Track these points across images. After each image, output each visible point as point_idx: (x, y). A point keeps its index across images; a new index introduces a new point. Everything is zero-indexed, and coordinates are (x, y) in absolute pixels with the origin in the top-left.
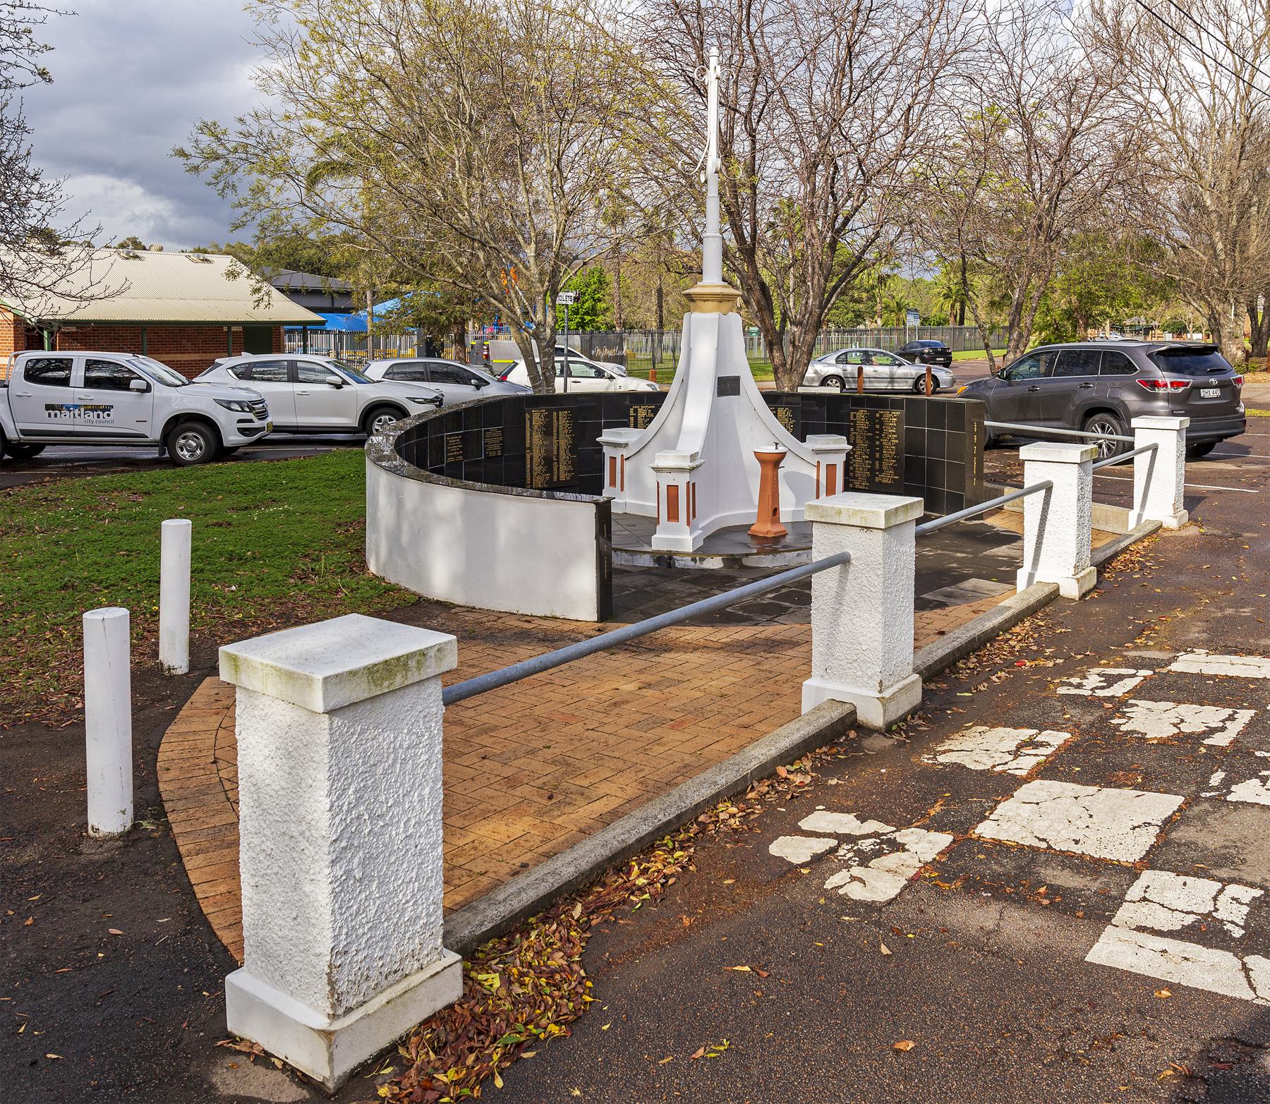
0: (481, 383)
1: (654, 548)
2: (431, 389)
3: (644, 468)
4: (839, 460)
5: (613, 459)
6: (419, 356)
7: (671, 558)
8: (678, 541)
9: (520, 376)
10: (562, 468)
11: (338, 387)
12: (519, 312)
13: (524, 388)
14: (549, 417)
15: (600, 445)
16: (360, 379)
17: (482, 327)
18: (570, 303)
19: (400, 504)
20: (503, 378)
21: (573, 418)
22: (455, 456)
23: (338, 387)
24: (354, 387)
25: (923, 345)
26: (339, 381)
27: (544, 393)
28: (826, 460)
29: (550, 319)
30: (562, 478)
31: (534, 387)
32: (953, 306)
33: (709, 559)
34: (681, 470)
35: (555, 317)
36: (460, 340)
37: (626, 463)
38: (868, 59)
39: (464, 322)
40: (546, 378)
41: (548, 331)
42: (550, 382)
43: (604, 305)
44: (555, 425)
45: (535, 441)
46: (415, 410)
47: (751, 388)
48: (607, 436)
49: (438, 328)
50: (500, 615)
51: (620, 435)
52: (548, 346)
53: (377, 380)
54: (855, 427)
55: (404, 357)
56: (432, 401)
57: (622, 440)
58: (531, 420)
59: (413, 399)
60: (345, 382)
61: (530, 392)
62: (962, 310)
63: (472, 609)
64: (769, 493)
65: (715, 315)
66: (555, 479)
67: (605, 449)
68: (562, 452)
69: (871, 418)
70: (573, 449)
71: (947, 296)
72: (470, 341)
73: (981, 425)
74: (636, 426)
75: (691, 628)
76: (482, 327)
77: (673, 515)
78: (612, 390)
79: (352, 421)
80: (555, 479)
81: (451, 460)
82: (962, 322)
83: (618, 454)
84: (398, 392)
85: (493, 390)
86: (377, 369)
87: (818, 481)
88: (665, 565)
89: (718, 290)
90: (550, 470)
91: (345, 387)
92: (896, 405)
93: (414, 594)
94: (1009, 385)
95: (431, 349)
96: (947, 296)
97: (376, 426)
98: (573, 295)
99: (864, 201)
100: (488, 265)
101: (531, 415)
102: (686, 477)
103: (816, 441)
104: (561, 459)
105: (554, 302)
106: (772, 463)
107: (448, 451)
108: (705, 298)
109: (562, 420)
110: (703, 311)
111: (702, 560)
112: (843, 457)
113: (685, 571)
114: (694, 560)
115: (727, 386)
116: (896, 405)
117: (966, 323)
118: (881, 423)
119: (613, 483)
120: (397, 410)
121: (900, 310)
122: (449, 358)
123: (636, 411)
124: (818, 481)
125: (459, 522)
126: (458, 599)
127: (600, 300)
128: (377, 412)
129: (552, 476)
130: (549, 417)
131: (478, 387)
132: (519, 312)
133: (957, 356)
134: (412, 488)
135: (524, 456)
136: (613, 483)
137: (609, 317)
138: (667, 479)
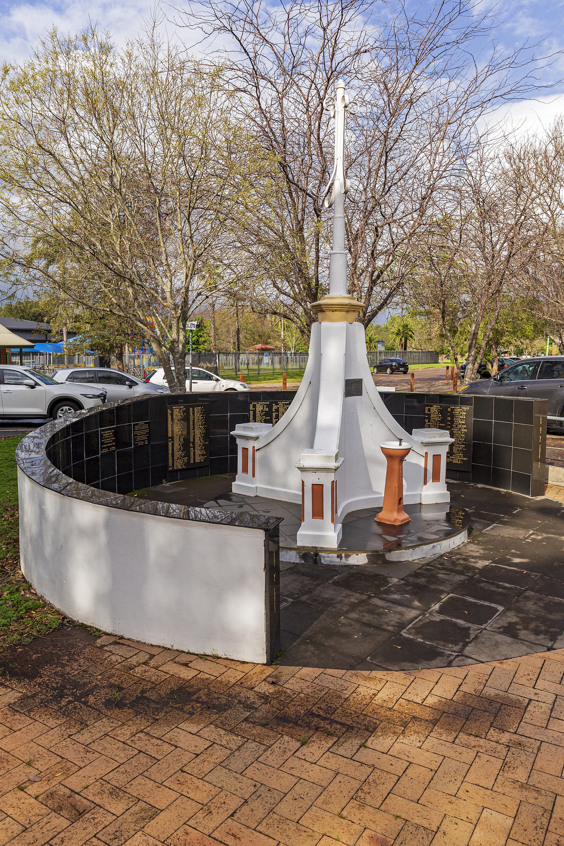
0: (133, 384)
1: (299, 544)
2: (99, 388)
3: (279, 463)
4: (443, 451)
5: (245, 450)
6: (95, 366)
7: (316, 555)
8: (321, 537)
9: (159, 378)
10: (198, 452)
11: (32, 387)
12: (159, 333)
13: (162, 387)
14: (187, 412)
15: (233, 439)
16: (50, 382)
17: (134, 351)
18: (194, 329)
19: (42, 513)
20: (147, 381)
21: (206, 413)
22: (108, 447)
23: (32, 387)
24: (43, 387)
25: (392, 361)
26: (31, 382)
27: (178, 392)
28: (432, 451)
29: (181, 338)
30: (197, 460)
31: (170, 387)
32: (401, 340)
33: (354, 556)
34: (327, 470)
35: (185, 336)
36: (120, 357)
37: (257, 454)
38: (399, 161)
39: (122, 347)
40: (179, 381)
41: (181, 346)
42: (182, 384)
43: (204, 339)
44: (191, 418)
45: (175, 428)
46: (88, 404)
47: (372, 390)
48: (239, 430)
49: (106, 353)
50: (154, 652)
51: (251, 429)
52: (180, 357)
53: (62, 383)
54: (429, 419)
55: (88, 367)
56: (98, 396)
57: (253, 434)
58: (172, 415)
59: (85, 395)
60: (37, 384)
61: (168, 392)
62: (406, 342)
63: (120, 641)
64: (396, 484)
65: (343, 324)
66: (192, 461)
67: (238, 441)
68: (197, 440)
69: (443, 412)
70: (206, 436)
71: (397, 334)
72: (126, 359)
73: (544, 419)
74: (255, 420)
75: (378, 674)
76: (134, 351)
77: (318, 513)
78: (217, 390)
79: (42, 410)
80: (192, 461)
81: (106, 450)
82: (405, 349)
83: (250, 445)
84: (75, 390)
85: (140, 390)
86: (62, 375)
87: (426, 469)
88: (311, 562)
89: (347, 301)
90: (188, 455)
91: (38, 388)
92: (464, 401)
93: (58, 612)
94: (501, 385)
95: (103, 362)
96: (397, 334)
97: (60, 413)
98: (196, 323)
99: (392, 261)
100: (136, 299)
101: (172, 410)
102: (331, 477)
103: (422, 435)
104: (197, 446)
105: (184, 325)
106: (395, 459)
107: (102, 443)
108: (334, 308)
109: (197, 414)
110: (331, 320)
111: (347, 556)
112: (446, 449)
113: (332, 569)
114: (340, 557)
115: (353, 388)
116: (464, 401)
117: (408, 350)
118: (452, 416)
119: (245, 470)
120: (76, 404)
121: (371, 342)
122: (114, 369)
123: (254, 406)
124: (426, 469)
125: (103, 537)
126: (104, 624)
127: (201, 336)
128: (59, 405)
129: (189, 460)
130: (187, 412)
131: (130, 387)
132: (159, 333)
133: (411, 368)
134: (51, 499)
135: (167, 446)
136: (245, 470)
137: (206, 346)
138: (311, 479)
